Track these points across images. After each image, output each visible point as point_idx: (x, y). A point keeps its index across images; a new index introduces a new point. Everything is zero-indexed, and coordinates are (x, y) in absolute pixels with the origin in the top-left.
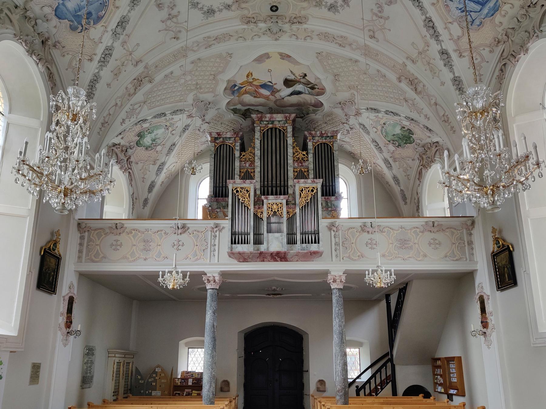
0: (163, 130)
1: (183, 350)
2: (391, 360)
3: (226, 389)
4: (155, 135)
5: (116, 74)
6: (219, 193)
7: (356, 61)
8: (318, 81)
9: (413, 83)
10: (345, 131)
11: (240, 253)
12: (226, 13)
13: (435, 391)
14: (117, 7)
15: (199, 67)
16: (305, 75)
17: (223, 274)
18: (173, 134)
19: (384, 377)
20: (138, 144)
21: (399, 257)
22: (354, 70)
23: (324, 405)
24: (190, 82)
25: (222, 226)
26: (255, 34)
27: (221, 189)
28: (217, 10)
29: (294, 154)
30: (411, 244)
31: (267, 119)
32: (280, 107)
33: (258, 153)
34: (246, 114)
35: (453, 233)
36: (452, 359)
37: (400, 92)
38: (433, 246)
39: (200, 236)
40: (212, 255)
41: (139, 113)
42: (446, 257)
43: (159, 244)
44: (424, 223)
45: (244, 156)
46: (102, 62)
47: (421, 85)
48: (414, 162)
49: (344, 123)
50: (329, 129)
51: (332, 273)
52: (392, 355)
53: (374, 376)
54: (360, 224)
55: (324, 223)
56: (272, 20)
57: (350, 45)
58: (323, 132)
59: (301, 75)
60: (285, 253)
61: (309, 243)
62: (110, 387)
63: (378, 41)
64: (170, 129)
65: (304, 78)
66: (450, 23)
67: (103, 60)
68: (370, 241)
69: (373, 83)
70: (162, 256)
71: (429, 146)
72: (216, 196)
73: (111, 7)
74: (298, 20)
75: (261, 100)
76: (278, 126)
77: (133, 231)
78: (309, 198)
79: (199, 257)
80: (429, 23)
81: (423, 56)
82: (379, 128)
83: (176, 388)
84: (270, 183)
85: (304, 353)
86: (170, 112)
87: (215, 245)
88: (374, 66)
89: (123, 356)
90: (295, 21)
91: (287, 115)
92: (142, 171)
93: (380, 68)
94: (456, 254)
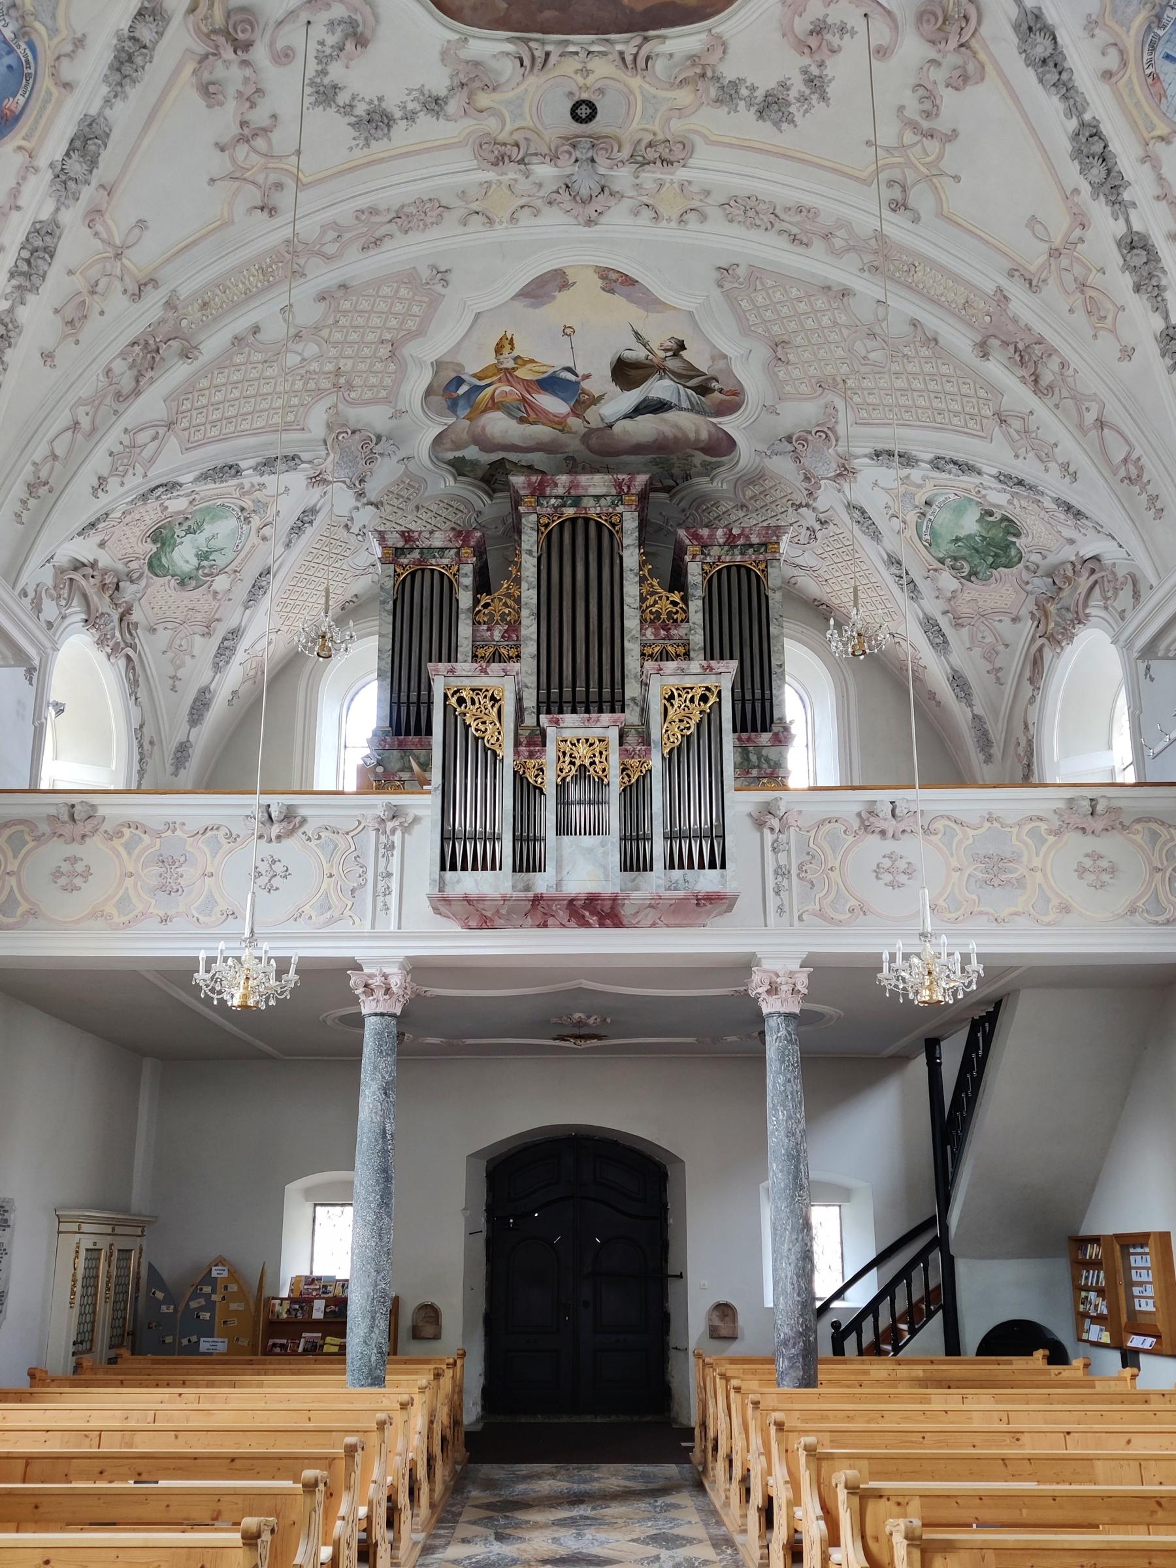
0: (232, 523)
1: (296, 1211)
2: (941, 1242)
3: (429, 1330)
4: (208, 540)
5: (74, 320)
6: (407, 721)
7: (845, 293)
8: (721, 364)
9: (1028, 356)
10: (804, 531)
11: (468, 900)
12: (428, 128)
13: (1080, 1340)
14: (67, 86)
15: (345, 313)
16: (681, 346)
17: (417, 969)
18: (264, 539)
19: (918, 1293)
20: (155, 565)
21: (981, 913)
22: (835, 323)
23: (738, 1390)
24: (315, 366)
25: (412, 813)
26: (523, 201)
27: (413, 709)
28: (398, 114)
29: (643, 599)
30: (1022, 870)
31: (560, 491)
32: (601, 452)
33: (529, 595)
34: (492, 477)
35: (1155, 836)
36: (1141, 1239)
37: (982, 393)
38: (1091, 877)
39: (342, 845)
40: (380, 905)
41: (152, 460)
42: (1133, 911)
43: (209, 870)
44: (1061, 805)
45: (486, 606)
46: (22, 274)
47: (1054, 364)
48: (1019, 625)
49: (800, 506)
50: (752, 523)
51: (766, 965)
52: (945, 1229)
53: (887, 1291)
54: (857, 808)
55: (740, 803)
56: (578, 154)
57: (826, 237)
58: (735, 532)
59: (668, 344)
60: (614, 899)
61: (691, 866)
62: (63, 1325)
63: (916, 220)
64: (256, 521)
65: (676, 354)
66: (1162, 138)
67: (24, 267)
68: (887, 863)
69: (895, 367)
70: (217, 910)
71: (1070, 573)
72: (398, 733)
73: (45, 83)
74: (661, 153)
75: (541, 432)
76: (593, 512)
77: (126, 831)
78: (693, 723)
79: (336, 914)
80: (1091, 145)
81: (1065, 262)
82: (912, 517)
83: (275, 1327)
84: (567, 690)
85: (671, 1221)
86: (252, 462)
87: (389, 875)
88: (903, 306)
89: (109, 1230)
90: (651, 154)
91: (620, 477)
92: (170, 655)
93: (921, 315)
94: (1165, 903)
